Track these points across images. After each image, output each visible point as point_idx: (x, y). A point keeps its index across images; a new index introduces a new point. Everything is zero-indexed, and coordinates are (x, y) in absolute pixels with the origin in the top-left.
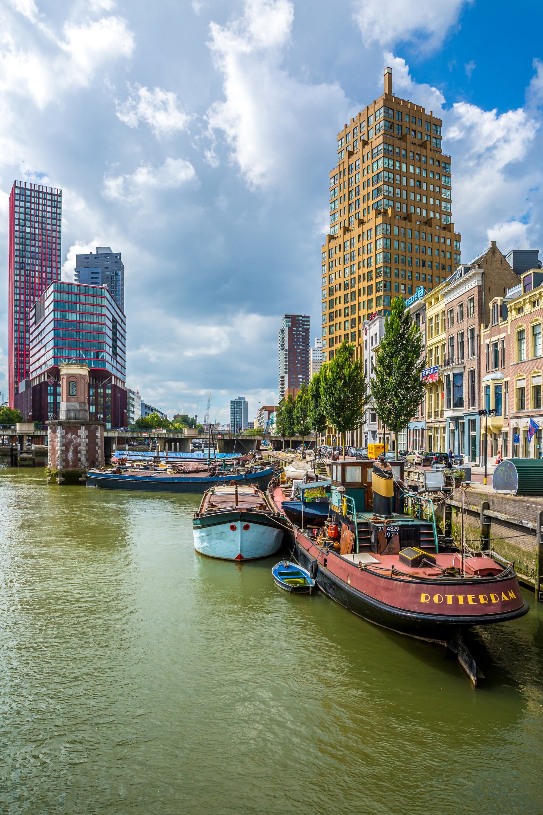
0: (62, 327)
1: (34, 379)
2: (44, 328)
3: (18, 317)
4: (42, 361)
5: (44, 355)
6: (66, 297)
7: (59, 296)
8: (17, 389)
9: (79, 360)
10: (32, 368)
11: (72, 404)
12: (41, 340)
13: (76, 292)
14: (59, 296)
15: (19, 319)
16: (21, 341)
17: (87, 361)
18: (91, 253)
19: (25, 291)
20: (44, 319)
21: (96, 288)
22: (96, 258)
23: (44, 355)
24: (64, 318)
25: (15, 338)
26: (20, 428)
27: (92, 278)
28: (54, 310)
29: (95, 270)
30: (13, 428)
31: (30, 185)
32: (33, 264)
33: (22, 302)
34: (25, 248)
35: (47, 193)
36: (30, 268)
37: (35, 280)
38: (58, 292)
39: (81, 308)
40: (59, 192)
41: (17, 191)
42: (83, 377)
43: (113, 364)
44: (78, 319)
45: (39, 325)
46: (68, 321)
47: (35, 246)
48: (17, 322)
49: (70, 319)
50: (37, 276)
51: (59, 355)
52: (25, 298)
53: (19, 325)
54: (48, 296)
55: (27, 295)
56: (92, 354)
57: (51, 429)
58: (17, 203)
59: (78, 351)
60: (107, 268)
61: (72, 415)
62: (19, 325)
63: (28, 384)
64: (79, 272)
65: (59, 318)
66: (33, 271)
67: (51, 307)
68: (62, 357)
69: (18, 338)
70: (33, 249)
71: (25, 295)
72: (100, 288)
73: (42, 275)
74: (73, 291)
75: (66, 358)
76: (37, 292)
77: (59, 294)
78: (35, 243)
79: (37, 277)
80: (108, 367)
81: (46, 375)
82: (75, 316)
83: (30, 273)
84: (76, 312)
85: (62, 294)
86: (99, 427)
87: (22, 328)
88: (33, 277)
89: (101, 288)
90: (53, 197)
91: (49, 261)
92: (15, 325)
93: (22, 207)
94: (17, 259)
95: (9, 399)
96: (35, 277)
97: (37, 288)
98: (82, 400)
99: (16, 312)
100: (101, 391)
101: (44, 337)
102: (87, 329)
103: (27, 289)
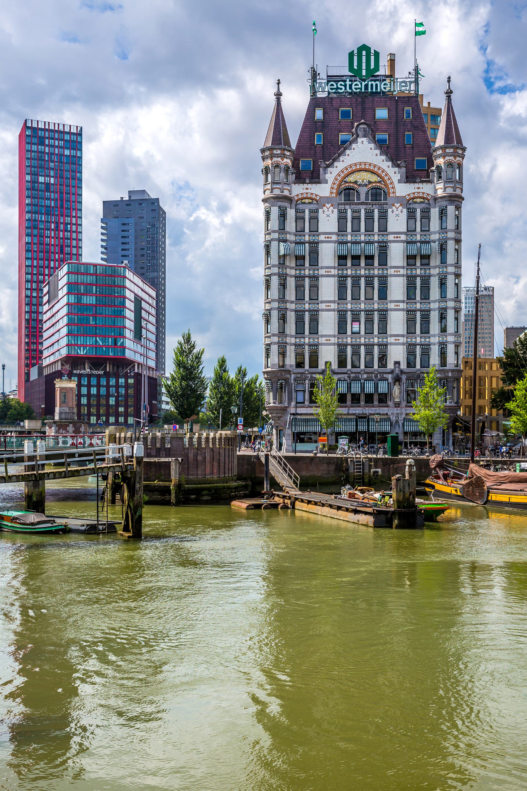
0: (76, 312)
1: (47, 366)
2: (58, 311)
3: (29, 287)
4: (56, 347)
5: (58, 341)
6: (81, 279)
7: (73, 278)
8: (28, 374)
9: (96, 347)
10: (45, 354)
11: (64, 409)
12: (55, 323)
13: (92, 272)
14: (73, 278)
15: (31, 289)
16: (34, 316)
17: (104, 348)
18: (122, 198)
19: (38, 255)
20: (58, 301)
21: (115, 266)
22: (127, 205)
23: (58, 341)
24: (79, 303)
25: (26, 312)
26: (29, 424)
27: (123, 231)
28: (68, 294)
29: (126, 221)
30: (22, 424)
31: (43, 123)
32: (47, 222)
33: (35, 269)
34: (38, 202)
35: (64, 133)
36: (45, 226)
37: (50, 241)
38: (72, 273)
39: (98, 290)
40: (79, 129)
41: (28, 133)
42: (71, 389)
43: (136, 349)
44: (94, 303)
45: (53, 306)
46: (84, 304)
47: (50, 199)
48: (29, 293)
49: (85, 302)
50: (53, 235)
51: (73, 343)
52: (38, 263)
53: (31, 297)
54: (62, 276)
55: (41, 259)
56: (110, 341)
57: (48, 426)
58: (28, 147)
59: (94, 338)
60: (142, 218)
61: (63, 416)
62: (31, 297)
63: (41, 370)
64: (106, 224)
65: (73, 302)
66: (48, 229)
67: (65, 290)
68: (77, 345)
69: (30, 312)
70: (47, 202)
71: (38, 259)
72: (119, 267)
73: (59, 234)
74: (88, 272)
75: (81, 345)
76: (53, 255)
77: (74, 275)
78: (50, 195)
79: (52, 238)
80: (128, 354)
81: (59, 363)
82: (91, 299)
83: (44, 233)
84: (92, 295)
85: (76, 275)
86: (83, 425)
87: (34, 301)
88: (47, 237)
89: (121, 267)
90: (72, 136)
91: (68, 216)
92: (27, 296)
93: (34, 152)
94: (28, 216)
95: (19, 386)
96: (50, 237)
97: (53, 250)
98: (71, 405)
99: (27, 281)
100: (122, 381)
101: (58, 321)
102: (104, 314)
103: (41, 252)
